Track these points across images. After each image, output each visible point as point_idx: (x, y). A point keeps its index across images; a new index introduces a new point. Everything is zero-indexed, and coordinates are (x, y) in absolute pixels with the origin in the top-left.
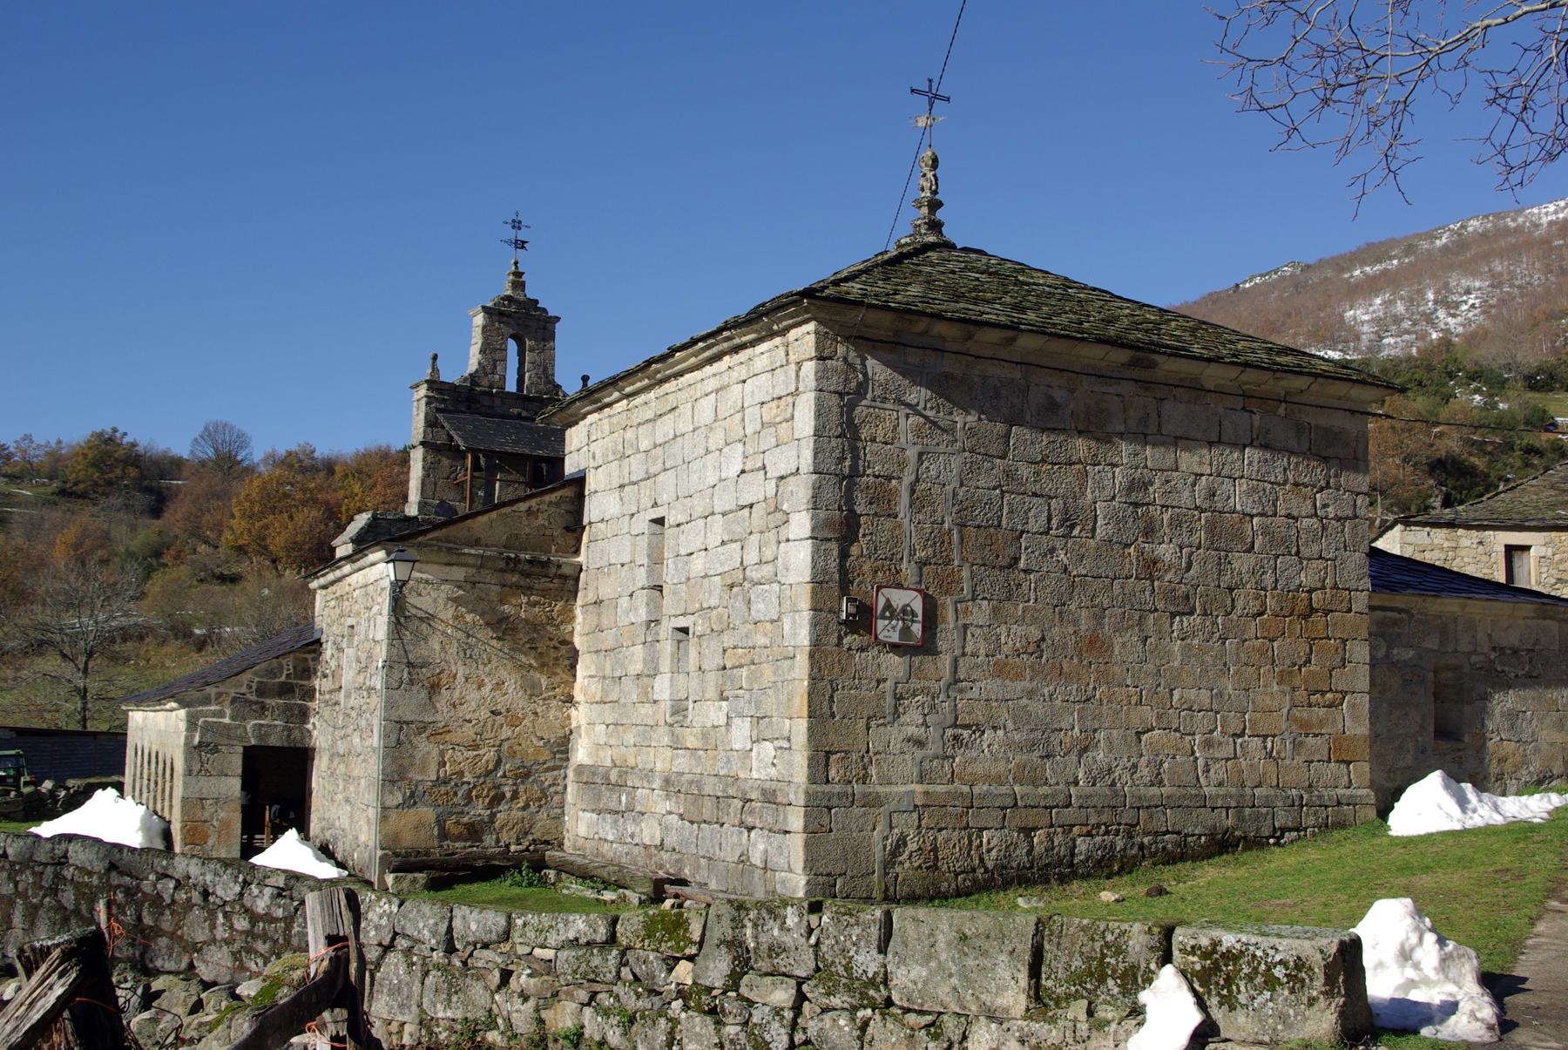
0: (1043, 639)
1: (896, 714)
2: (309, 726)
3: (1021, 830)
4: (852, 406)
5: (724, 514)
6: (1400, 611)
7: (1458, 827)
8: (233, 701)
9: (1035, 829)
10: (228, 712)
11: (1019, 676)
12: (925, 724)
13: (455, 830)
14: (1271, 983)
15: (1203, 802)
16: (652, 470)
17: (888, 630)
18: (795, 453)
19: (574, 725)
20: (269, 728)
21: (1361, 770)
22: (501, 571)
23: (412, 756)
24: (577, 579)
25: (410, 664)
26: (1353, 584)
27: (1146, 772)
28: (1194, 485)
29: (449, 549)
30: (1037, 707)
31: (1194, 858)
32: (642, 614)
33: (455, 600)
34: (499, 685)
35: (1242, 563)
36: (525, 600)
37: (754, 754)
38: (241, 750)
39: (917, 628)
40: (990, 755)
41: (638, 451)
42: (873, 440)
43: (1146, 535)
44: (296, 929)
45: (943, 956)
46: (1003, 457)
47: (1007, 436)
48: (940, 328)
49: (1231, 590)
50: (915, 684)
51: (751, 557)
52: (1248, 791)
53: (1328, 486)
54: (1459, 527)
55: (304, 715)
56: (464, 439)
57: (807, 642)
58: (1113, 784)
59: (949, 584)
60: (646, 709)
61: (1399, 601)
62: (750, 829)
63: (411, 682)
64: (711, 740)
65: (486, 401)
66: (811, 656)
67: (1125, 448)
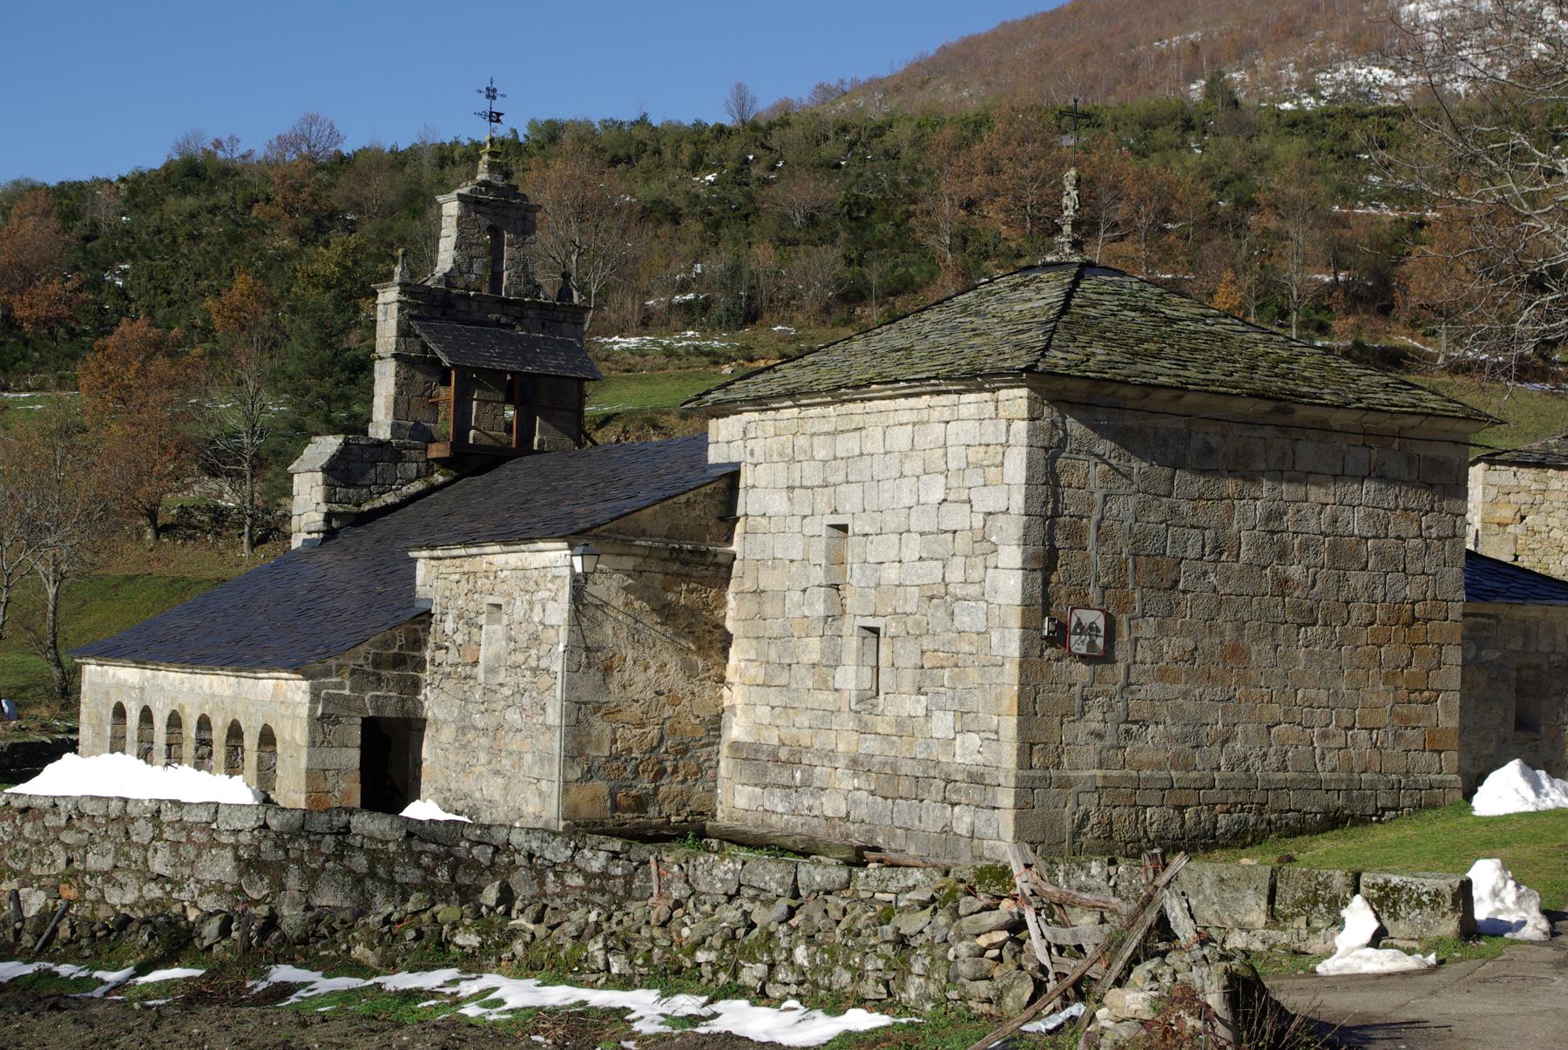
0: (1196, 649)
1: (1083, 713)
2: (421, 697)
3: (1176, 807)
4: (1054, 459)
5: (921, 534)
6: (1489, 616)
7: (1532, 809)
8: (353, 672)
9: (1187, 807)
10: (348, 683)
11: (1176, 680)
12: (1104, 721)
13: (625, 802)
14: (1420, 904)
15: (1319, 785)
16: (831, 480)
17: (1078, 644)
18: (1005, 496)
19: (726, 703)
20: (380, 699)
21: (1451, 758)
22: (665, 560)
23: (589, 734)
24: (730, 567)
25: (587, 649)
26: (1450, 596)
27: (1274, 759)
28: (1320, 513)
29: (623, 541)
30: (1190, 705)
31: (1312, 832)
32: (820, 609)
33: (625, 589)
34: (663, 666)
35: (1357, 579)
36: (684, 587)
37: (958, 742)
38: (359, 721)
39: (1100, 642)
40: (1153, 744)
41: (813, 458)
42: (1070, 486)
43: (1280, 558)
44: (637, 883)
45: (1208, 892)
46: (1168, 496)
47: (1173, 478)
48: (1125, 391)
49: (1348, 603)
50: (1098, 688)
51: (955, 575)
52: (1356, 776)
53: (1432, 510)
54: (1550, 467)
55: (416, 686)
56: (448, 354)
57: (1017, 654)
58: (1248, 770)
59: (1124, 604)
60: (826, 697)
61: (1488, 608)
62: (953, 805)
63: (589, 665)
64: (903, 727)
65: (462, 306)
66: (1021, 666)
67: (1266, 485)
